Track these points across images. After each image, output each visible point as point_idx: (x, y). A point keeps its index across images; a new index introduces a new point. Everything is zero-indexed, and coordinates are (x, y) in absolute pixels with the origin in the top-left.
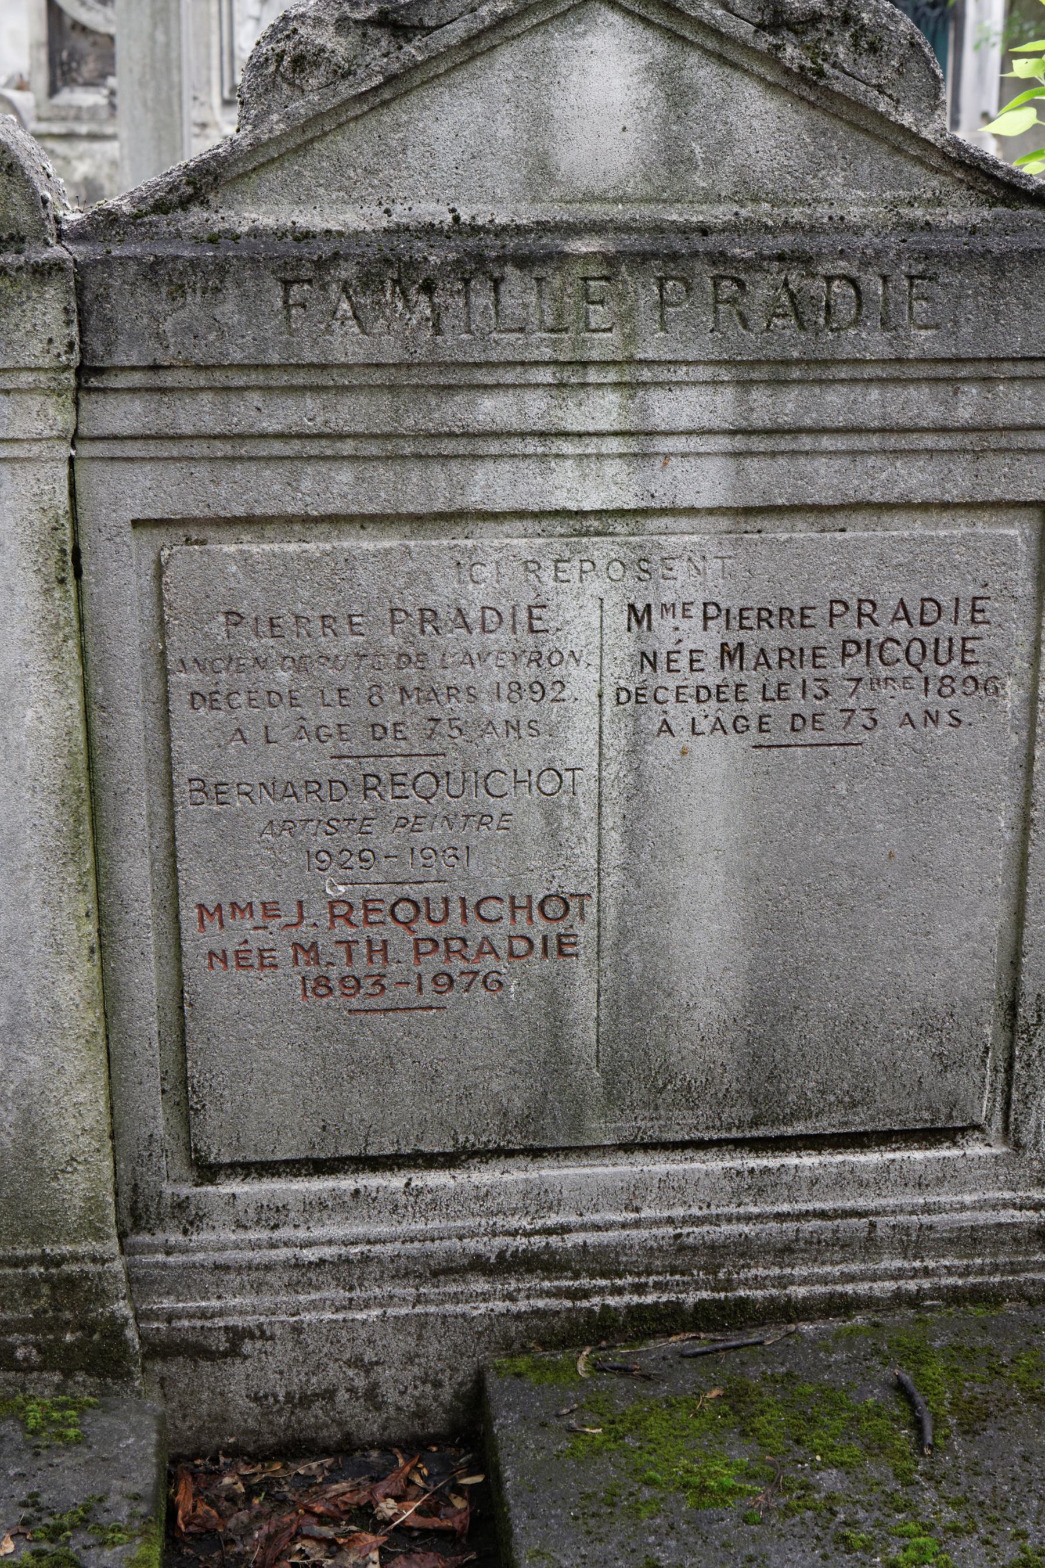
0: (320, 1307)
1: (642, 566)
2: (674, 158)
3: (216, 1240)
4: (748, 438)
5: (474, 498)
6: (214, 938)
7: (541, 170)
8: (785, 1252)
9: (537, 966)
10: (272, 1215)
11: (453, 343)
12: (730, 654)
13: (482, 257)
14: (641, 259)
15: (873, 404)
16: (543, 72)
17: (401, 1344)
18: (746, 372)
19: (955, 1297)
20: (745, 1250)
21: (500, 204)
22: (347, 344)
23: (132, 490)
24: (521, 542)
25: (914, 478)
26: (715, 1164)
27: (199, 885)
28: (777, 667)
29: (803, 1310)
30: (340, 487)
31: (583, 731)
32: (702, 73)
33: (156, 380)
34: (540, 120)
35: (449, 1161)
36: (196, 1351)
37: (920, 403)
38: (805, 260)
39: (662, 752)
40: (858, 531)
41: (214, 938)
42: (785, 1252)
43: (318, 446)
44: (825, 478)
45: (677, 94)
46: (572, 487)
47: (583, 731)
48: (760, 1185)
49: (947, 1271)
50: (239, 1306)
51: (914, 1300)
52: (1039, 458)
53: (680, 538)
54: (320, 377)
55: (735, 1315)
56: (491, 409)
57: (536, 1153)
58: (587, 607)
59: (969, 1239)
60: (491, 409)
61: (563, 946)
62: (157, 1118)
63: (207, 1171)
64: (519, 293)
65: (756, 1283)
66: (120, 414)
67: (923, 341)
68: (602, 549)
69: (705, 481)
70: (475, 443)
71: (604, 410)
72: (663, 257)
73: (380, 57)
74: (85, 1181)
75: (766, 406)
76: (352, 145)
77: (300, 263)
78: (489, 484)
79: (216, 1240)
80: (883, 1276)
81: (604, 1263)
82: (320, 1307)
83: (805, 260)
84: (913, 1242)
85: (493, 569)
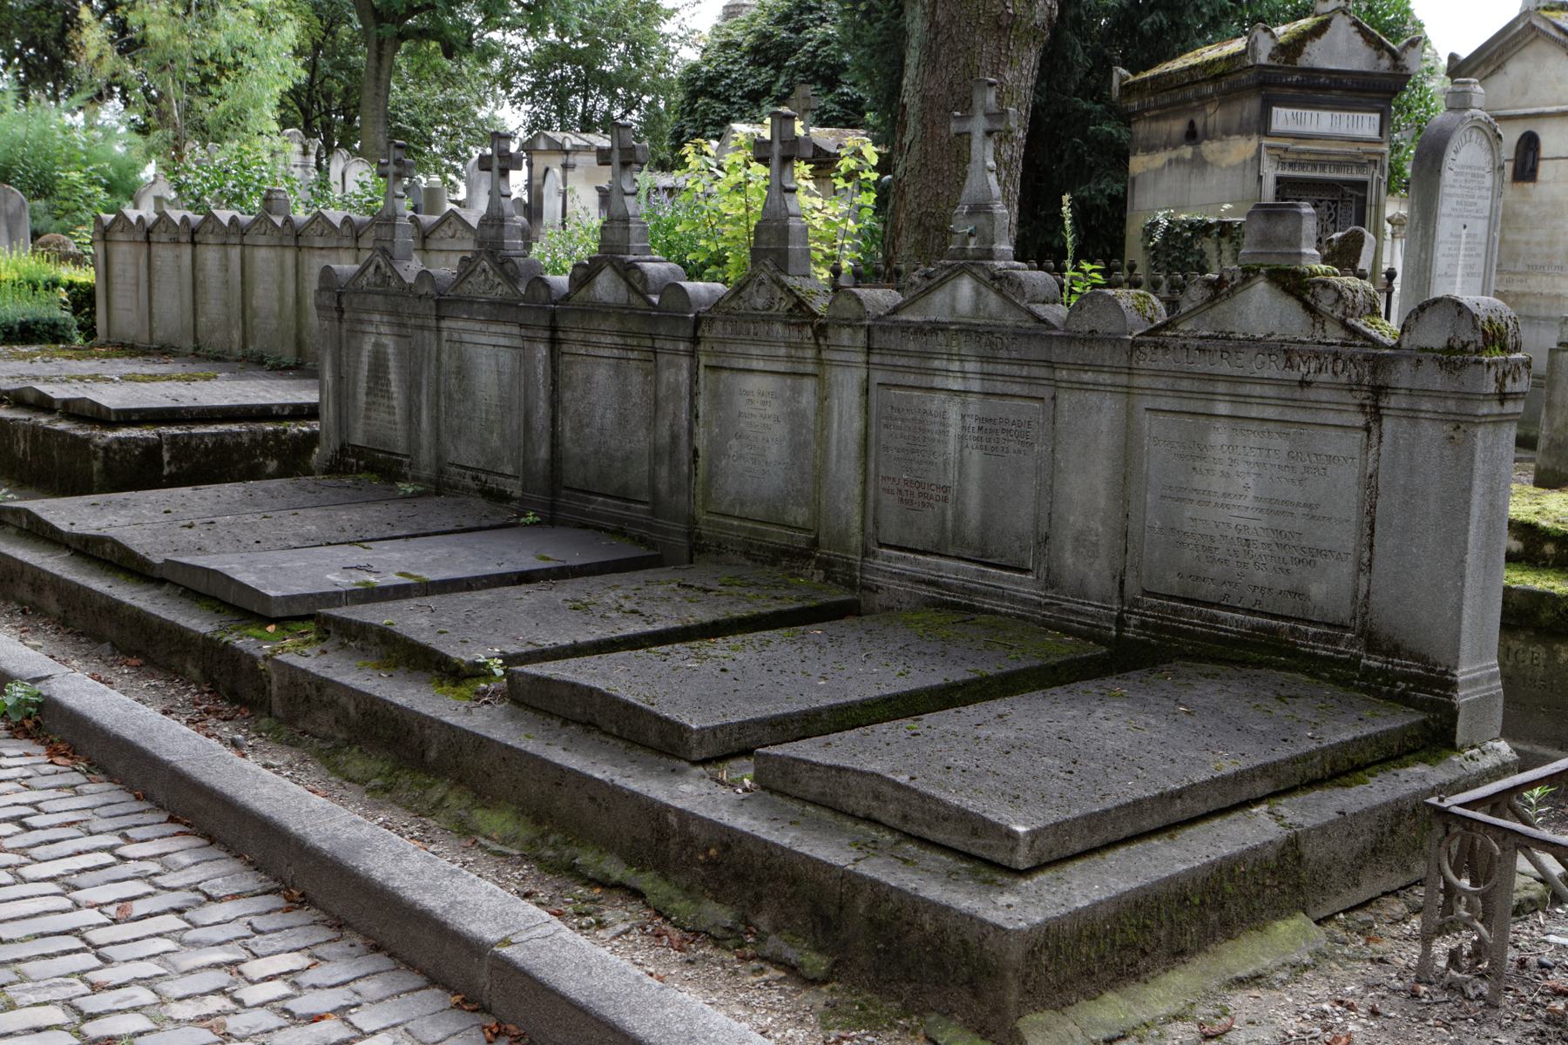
0: (893, 584)
1: (964, 403)
2: (976, 308)
3: (879, 563)
4: (985, 376)
5: (736, 365)
6: (882, 484)
7: (953, 309)
8: (985, 594)
9: (941, 504)
10: (889, 559)
11: (929, 348)
12: (980, 429)
13: (936, 328)
14: (962, 331)
15: (1006, 369)
16: (955, 287)
17: (906, 598)
18: (984, 359)
19: (1019, 617)
20: (975, 592)
21: (944, 318)
22: (911, 346)
23: (878, 376)
24: (943, 396)
25: (1016, 389)
26: (974, 567)
27: (882, 470)
28: (990, 432)
29: (985, 611)
30: (911, 379)
31: (952, 446)
32: (983, 289)
33: (882, 351)
34: (954, 299)
35: (924, 553)
36: (870, 590)
37: (1015, 370)
38: (991, 333)
39: (966, 452)
40: (1008, 402)
41: (882, 484)
42: (985, 594)
43: (907, 369)
44: (999, 387)
45: (978, 293)
46: (956, 385)
47: (952, 446)
48: (983, 575)
49: (1019, 609)
50: (880, 580)
51: (1009, 615)
52: (16, 309)
53: (972, 399)
54: (906, 353)
55: (970, 608)
56: (937, 364)
57: (941, 556)
58: (954, 412)
59: (1024, 601)
60: (937, 364)
61: (945, 500)
62: (870, 528)
63: (881, 545)
64: (941, 338)
65: (978, 601)
66: (875, 359)
67: (1014, 354)
68: (957, 399)
69: (975, 385)
70: (934, 372)
71: (956, 366)
72: (969, 331)
73: (926, 283)
74: (856, 540)
75: (989, 368)
76: (922, 303)
77: (906, 327)
78: (938, 382)
79: (879, 563)
80: (1004, 607)
81: (948, 587)
82: (893, 584)
83: (991, 333)
84: (1013, 599)
85: (936, 402)
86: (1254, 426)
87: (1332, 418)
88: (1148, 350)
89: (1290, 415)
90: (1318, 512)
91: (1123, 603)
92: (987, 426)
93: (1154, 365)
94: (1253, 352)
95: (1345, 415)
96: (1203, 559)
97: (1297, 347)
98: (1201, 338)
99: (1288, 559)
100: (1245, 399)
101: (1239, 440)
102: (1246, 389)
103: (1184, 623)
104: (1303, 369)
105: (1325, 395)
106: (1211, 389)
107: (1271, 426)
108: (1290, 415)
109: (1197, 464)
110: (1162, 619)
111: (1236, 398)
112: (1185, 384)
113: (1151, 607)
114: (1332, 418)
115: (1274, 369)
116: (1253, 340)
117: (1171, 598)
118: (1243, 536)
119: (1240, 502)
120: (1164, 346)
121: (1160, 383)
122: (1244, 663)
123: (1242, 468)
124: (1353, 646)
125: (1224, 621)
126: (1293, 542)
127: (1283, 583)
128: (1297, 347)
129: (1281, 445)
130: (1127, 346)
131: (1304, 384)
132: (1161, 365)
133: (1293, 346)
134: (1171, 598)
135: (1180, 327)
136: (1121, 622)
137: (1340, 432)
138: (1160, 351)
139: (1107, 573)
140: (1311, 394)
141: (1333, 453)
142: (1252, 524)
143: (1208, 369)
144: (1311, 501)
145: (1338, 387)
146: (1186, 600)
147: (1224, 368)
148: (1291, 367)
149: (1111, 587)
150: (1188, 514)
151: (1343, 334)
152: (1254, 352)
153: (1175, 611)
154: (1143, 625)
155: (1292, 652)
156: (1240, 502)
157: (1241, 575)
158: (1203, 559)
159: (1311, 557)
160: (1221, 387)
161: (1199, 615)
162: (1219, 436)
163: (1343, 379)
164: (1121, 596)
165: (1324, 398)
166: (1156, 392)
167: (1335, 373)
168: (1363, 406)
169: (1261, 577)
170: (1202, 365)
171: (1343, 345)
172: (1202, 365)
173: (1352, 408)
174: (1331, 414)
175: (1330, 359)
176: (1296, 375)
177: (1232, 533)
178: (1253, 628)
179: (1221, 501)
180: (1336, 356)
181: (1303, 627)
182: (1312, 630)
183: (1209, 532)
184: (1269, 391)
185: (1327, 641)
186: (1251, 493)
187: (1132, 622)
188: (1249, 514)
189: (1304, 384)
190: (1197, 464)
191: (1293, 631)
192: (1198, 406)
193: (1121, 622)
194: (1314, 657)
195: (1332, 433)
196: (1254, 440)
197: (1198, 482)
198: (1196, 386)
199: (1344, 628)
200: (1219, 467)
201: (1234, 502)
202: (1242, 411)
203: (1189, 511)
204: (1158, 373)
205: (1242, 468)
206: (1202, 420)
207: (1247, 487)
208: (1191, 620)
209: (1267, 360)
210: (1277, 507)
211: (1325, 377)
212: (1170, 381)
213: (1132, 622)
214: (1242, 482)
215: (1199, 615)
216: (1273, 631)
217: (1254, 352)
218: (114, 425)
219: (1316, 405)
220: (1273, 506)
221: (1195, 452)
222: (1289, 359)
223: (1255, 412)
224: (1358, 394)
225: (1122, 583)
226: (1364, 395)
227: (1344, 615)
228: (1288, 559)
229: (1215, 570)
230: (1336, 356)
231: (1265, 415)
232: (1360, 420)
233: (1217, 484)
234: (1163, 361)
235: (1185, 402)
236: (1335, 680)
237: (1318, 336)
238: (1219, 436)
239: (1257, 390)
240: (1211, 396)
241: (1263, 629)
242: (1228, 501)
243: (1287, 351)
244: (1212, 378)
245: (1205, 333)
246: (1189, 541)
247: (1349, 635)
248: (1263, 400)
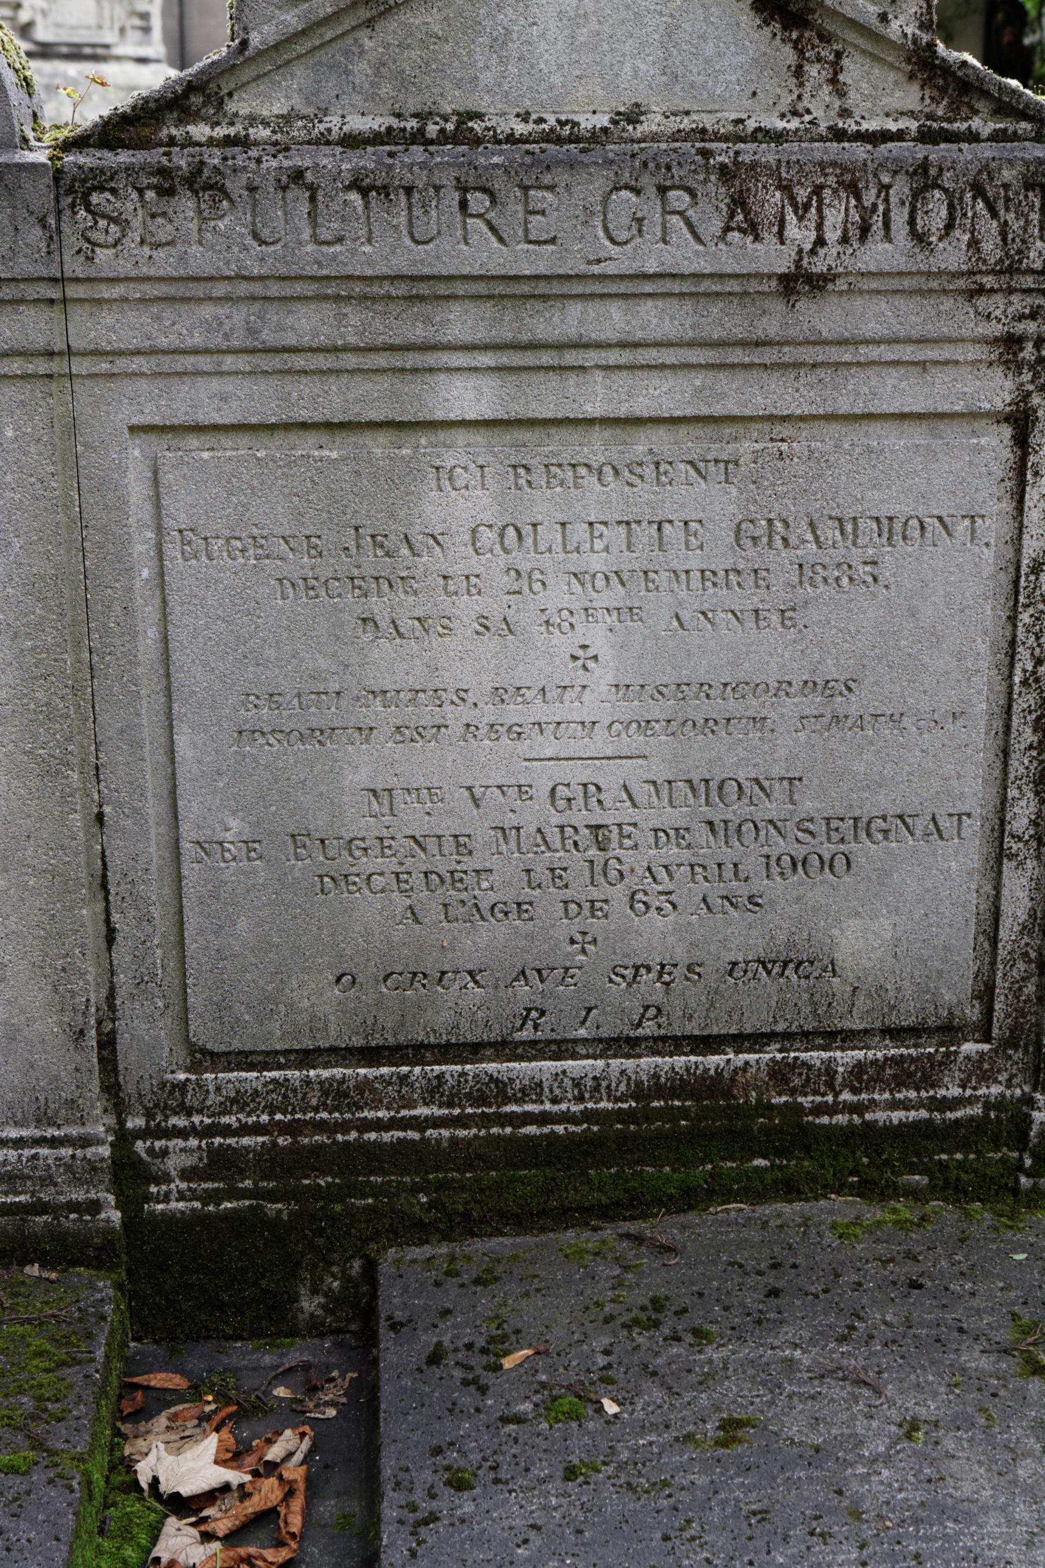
86: (596, 447)
87: (898, 392)
88: (129, 205)
89: (735, 395)
90: (852, 705)
91: (119, 1107)
92: (371, 561)
93: (165, 262)
94: (591, 186)
95: (941, 377)
96: (434, 913)
97: (767, 154)
98: (351, 141)
99: (752, 864)
100: (564, 357)
101: (543, 505)
102: (570, 320)
103: (380, 1126)
104: (800, 234)
105: (874, 316)
106: (419, 333)
107: (659, 439)
108: (735, 395)
109: (378, 606)
110: (292, 1129)
111: (519, 357)
112: (307, 323)
113: (238, 1101)
114: (898, 392)
115: (683, 241)
116: (563, 135)
117: (307, 1058)
118: (580, 817)
119: (570, 710)
120: (205, 185)
121: (186, 327)
122: (632, 1204)
123: (559, 595)
124: (987, 1078)
125: (534, 1089)
126: (771, 809)
127: (742, 937)
128: (767, 154)
129: (719, 503)
130: (40, 194)
131: (799, 283)
132: (200, 259)
133: (748, 152)
134: (307, 1058)
135: (240, 106)
136: (130, 1174)
137: (917, 435)
138: (186, 204)
139: (50, 1026)
140: (823, 316)
141: (901, 508)
142: (611, 777)
143: (409, 256)
144: (830, 670)
145: (928, 286)
146: (370, 1055)
147: (478, 252)
148: (752, 229)
149: (72, 1070)
150: (362, 777)
151: (911, 96)
152: (601, 181)
153: (336, 1094)
154: (221, 1164)
155: (793, 1135)
156: (570, 710)
157: (582, 941)
158: (434, 913)
159: (830, 846)
160: (461, 322)
161: (434, 1091)
162: (460, 499)
163: (952, 255)
164: (112, 1089)
165: (871, 328)
166: (169, 363)
167: (919, 238)
168: (1012, 342)
169: (657, 935)
170: (382, 247)
171: (926, 136)
172: (382, 247)
173: (975, 352)
174: (892, 377)
175: (901, 188)
176: (772, 257)
177: (535, 814)
178: (639, 1092)
179: (488, 713)
180: (925, 180)
181: (815, 1057)
182: (846, 1058)
183: (449, 826)
184: (655, 319)
185: (901, 1081)
186: (602, 677)
187: (173, 1164)
188: (600, 743)
189: (799, 283)
190: (378, 606)
191: (779, 1074)
192: (369, 397)
193: (130, 1174)
194: (871, 1135)
195: (896, 440)
196: (597, 498)
197: (388, 663)
198: (355, 324)
199: (950, 1031)
200: (466, 608)
201: (540, 711)
202: (547, 398)
203: (360, 767)
204: (184, 290)
205: (559, 595)
206: (378, 446)
207: (584, 657)
208: (410, 1110)
209: (650, 207)
210: (700, 709)
211: (879, 254)
212: (239, 316)
213: (173, 1164)
214: (563, 644)
215: (434, 1091)
216: (714, 1086)
217: (601, 181)
218: (265, 1067)
219: (844, 354)
220: (688, 705)
221: (368, 564)
222: (739, 202)
223: (596, 397)
224: (996, 304)
225: (108, 1043)
226: (1019, 304)
227: (956, 994)
228: (752, 864)
229: (485, 940)
230: (925, 180)
231: (641, 407)
232: (997, 390)
233: (466, 661)
234: (202, 241)
235: (306, 387)
236: (951, 1187)
237: (821, 108)
238: (460, 499)
239: (613, 320)
240: (415, 359)
241: (658, 1088)
242: (513, 713)
243: (732, 174)
244: (424, 290)
245: (359, 124)
246: (367, 864)
247: (969, 1048)
248: (633, 354)
